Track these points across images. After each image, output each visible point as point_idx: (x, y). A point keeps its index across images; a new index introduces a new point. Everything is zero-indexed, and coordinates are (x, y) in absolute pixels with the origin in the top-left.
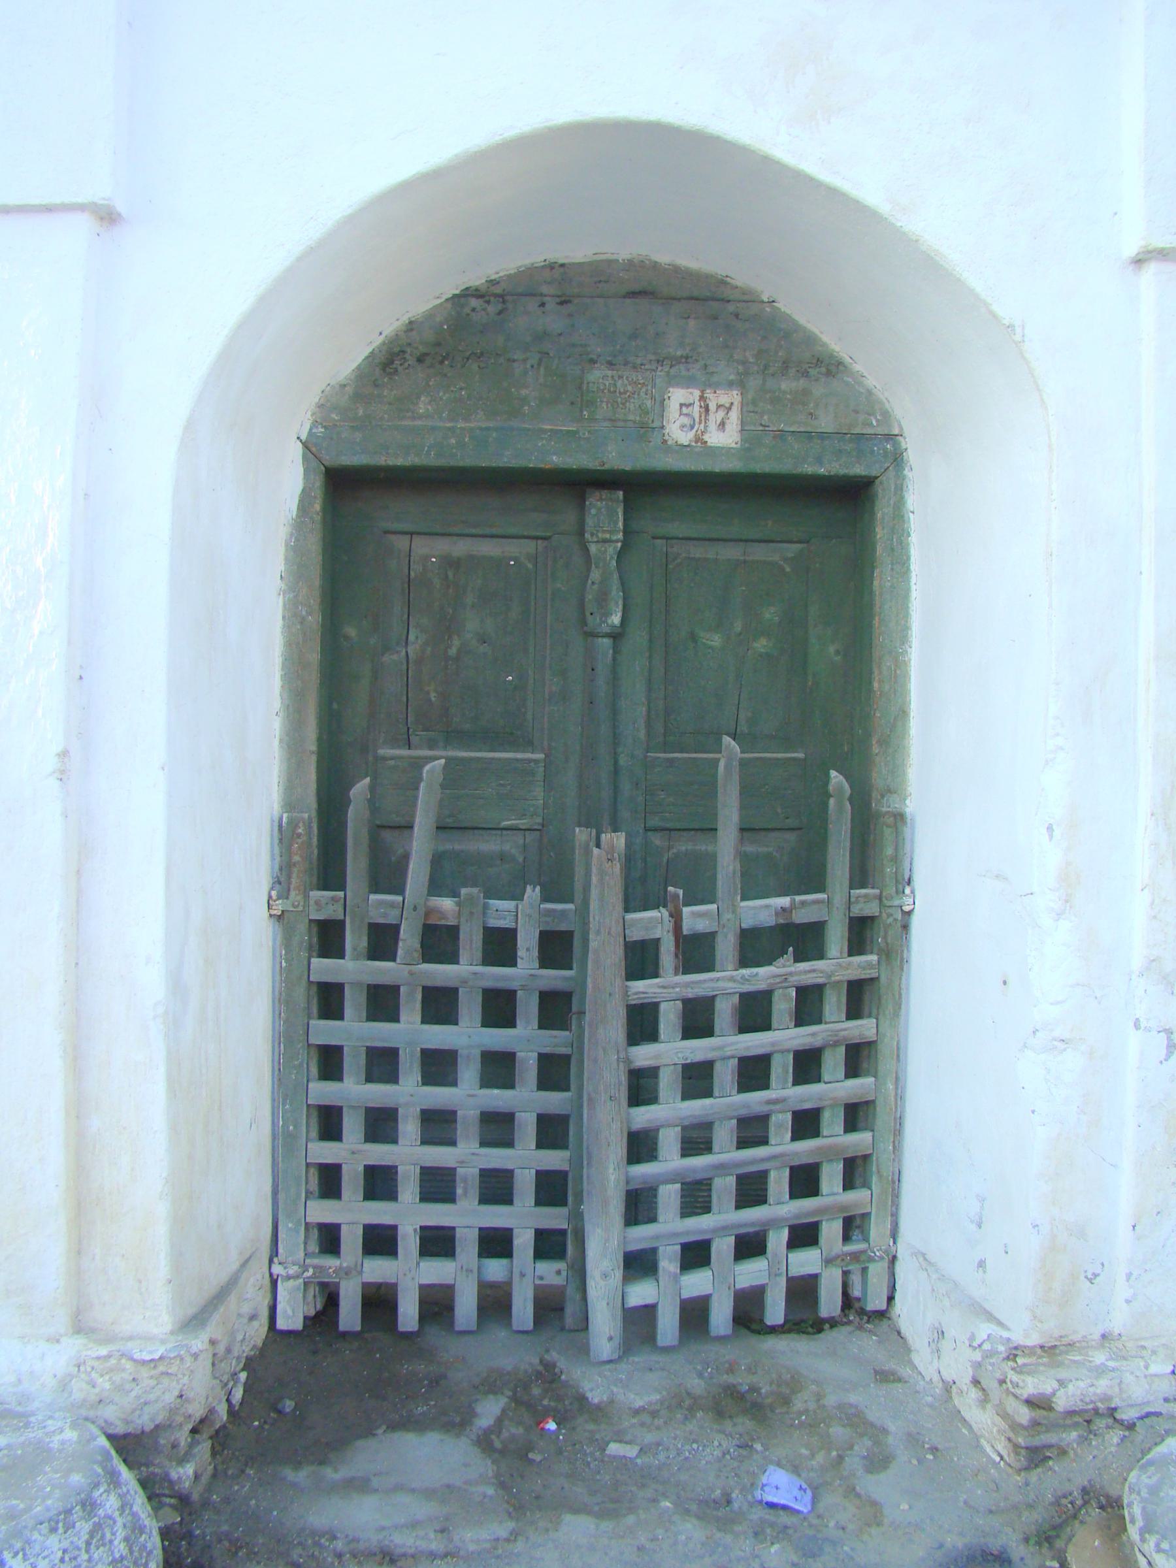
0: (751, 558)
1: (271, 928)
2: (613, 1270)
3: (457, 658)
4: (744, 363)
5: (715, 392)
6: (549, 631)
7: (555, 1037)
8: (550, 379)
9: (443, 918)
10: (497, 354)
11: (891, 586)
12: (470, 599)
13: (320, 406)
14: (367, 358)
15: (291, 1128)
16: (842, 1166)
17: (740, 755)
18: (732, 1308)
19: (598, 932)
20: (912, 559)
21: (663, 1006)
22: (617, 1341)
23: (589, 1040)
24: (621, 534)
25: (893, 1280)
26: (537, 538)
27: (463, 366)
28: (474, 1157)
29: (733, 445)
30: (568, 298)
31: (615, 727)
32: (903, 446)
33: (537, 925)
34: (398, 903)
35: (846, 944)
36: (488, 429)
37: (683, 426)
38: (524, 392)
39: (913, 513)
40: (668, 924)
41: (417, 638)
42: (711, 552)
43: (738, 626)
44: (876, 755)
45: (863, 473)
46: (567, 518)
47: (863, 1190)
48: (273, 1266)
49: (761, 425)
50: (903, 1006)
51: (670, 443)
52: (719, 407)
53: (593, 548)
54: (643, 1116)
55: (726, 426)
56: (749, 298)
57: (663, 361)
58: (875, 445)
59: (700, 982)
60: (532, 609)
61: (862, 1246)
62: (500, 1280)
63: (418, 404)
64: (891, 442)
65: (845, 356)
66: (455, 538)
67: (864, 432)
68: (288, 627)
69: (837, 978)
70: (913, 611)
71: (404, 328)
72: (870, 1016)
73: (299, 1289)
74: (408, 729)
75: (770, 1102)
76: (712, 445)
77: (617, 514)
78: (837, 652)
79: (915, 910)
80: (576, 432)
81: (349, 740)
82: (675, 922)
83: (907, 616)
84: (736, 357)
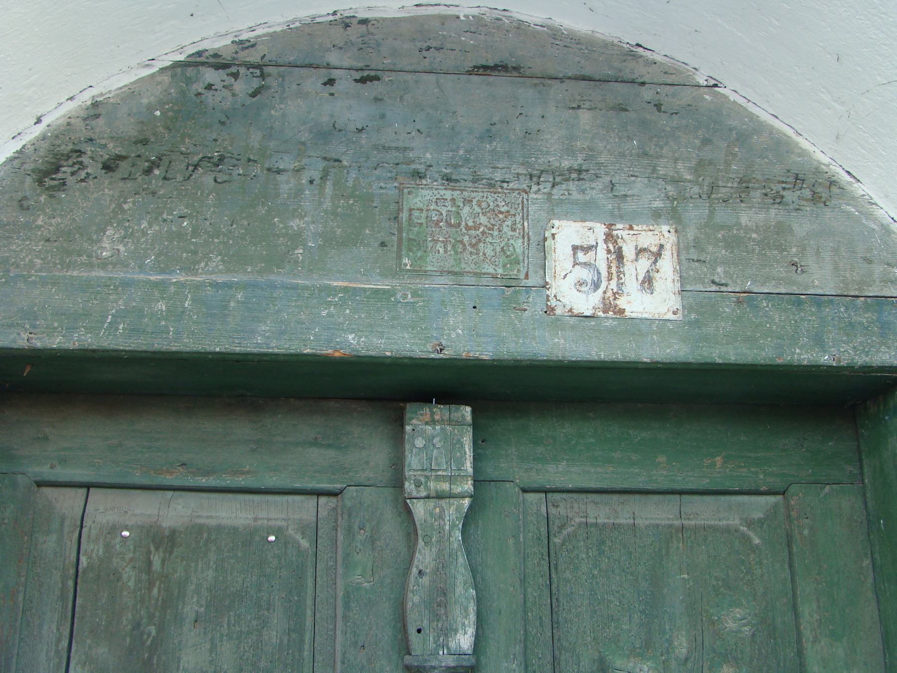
5: (631, 228)
10: (249, 160)
12: (191, 607)
14: (11, 160)
24: (470, 482)
26: (319, 493)
29: (670, 316)
30: (372, 73)
36: (228, 286)
38: (295, 224)
43: (682, 645)
49: (713, 282)
51: (559, 311)
52: (640, 251)
53: (419, 509)
57: (539, 177)
60: (309, 623)
63: (100, 241)
65: (839, 170)
66: (170, 494)
71: (83, 114)
76: (634, 315)
77: (462, 446)
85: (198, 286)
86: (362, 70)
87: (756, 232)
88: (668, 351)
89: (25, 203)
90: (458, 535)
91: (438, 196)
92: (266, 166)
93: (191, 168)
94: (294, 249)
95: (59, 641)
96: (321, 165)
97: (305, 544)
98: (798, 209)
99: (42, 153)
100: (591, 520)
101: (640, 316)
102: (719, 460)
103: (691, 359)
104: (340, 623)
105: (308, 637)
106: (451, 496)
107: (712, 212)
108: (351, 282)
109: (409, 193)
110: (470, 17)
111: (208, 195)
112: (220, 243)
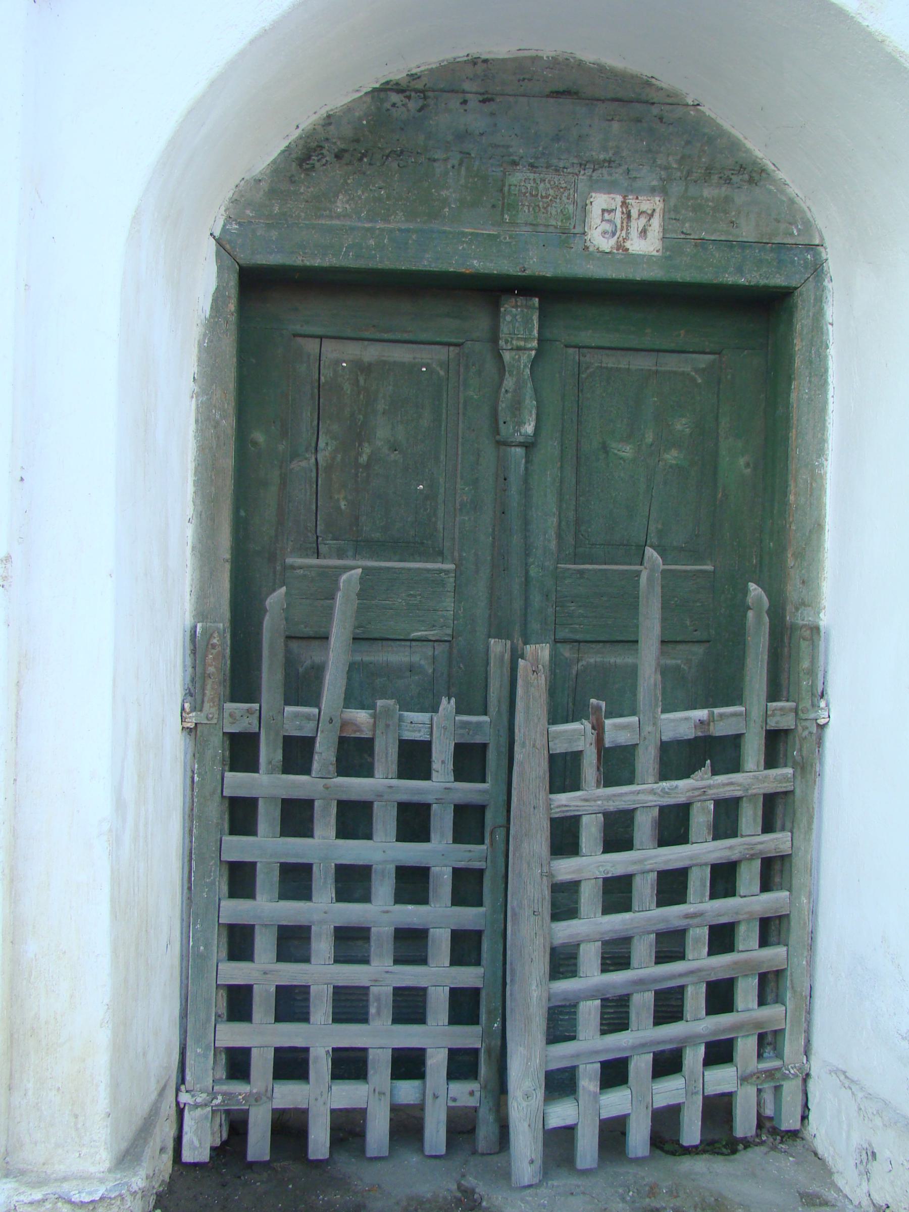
0: (663, 369)
1: (182, 742)
2: (534, 1090)
3: (368, 466)
4: (666, 168)
5: (637, 198)
6: (460, 440)
7: (470, 851)
8: (471, 180)
9: (359, 731)
10: (418, 153)
11: (809, 398)
12: (381, 406)
13: (234, 201)
14: (283, 152)
15: (202, 948)
16: (757, 980)
17: (662, 567)
18: (649, 1129)
19: (523, 745)
20: (830, 372)
21: (585, 820)
22: (539, 1162)
23: (514, 855)
24: (536, 342)
25: (805, 1099)
26: (449, 344)
27: (383, 164)
28: (388, 975)
29: (655, 253)
30: (489, 96)
31: (526, 538)
32: (824, 256)
33: (452, 738)
34: (314, 715)
35: (763, 757)
36: (408, 231)
37: (605, 233)
38: (444, 193)
39: (832, 324)
40: (591, 736)
41: (327, 444)
42: (623, 362)
43: (649, 438)
44: (792, 567)
45: (783, 284)
46: (480, 323)
47: (777, 1005)
48: (180, 1094)
49: (683, 233)
50: (815, 820)
51: (591, 249)
52: (641, 213)
53: (507, 356)
54: (565, 930)
55: (648, 234)
56: (674, 100)
57: (586, 165)
58: (796, 256)
59: (621, 795)
60: (444, 416)
61: (777, 1063)
62: (412, 1102)
63: (336, 202)
64: (811, 252)
65: (768, 162)
66: (366, 343)
67: (785, 241)
68: (201, 431)
69: (754, 791)
70: (829, 423)
71: (322, 122)
72: (783, 829)
73: (206, 1117)
74: (317, 537)
75: (687, 916)
76: (634, 252)
77: (532, 320)
78: (747, 465)
79: (829, 723)
80: (498, 236)
81: (257, 549)
82: (598, 734)
83: (823, 429)
84: (659, 162)
85: (391, 231)
86: (483, 94)
87: (711, 202)
88: (651, 274)
89: (293, 179)
90: (528, 371)
91: (526, 177)
92: (427, 157)
93: (384, 158)
94: (443, 209)
95: (312, 422)
96: (459, 156)
97: (442, 373)
98: (739, 188)
99: (300, 147)
100: (604, 365)
101: (637, 253)
102: (682, 332)
103: (664, 279)
104: (461, 416)
105: (444, 424)
106: (526, 349)
107: (686, 190)
108: (475, 229)
109: (510, 175)
110: (550, 58)
111: (395, 174)
112: (402, 204)
